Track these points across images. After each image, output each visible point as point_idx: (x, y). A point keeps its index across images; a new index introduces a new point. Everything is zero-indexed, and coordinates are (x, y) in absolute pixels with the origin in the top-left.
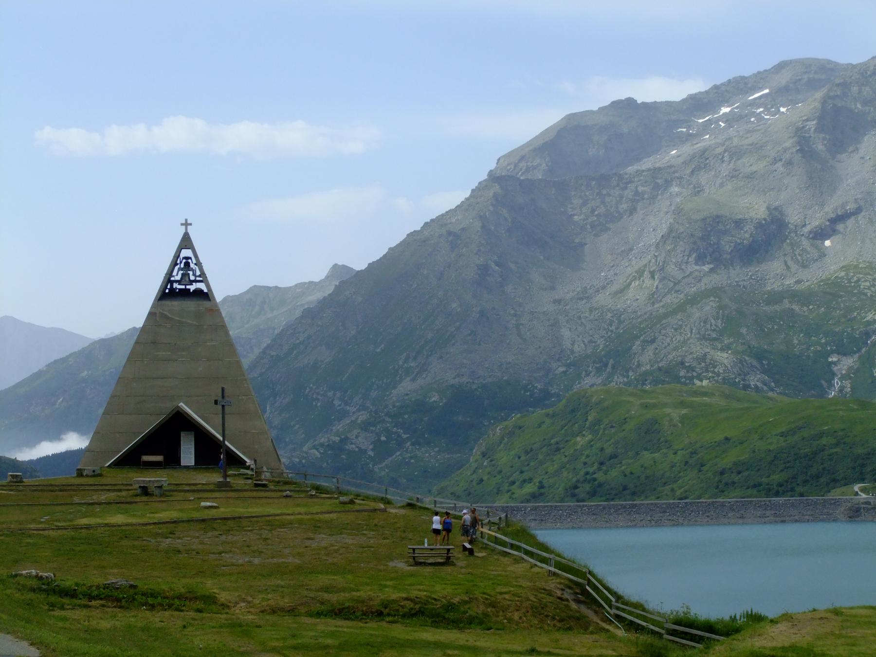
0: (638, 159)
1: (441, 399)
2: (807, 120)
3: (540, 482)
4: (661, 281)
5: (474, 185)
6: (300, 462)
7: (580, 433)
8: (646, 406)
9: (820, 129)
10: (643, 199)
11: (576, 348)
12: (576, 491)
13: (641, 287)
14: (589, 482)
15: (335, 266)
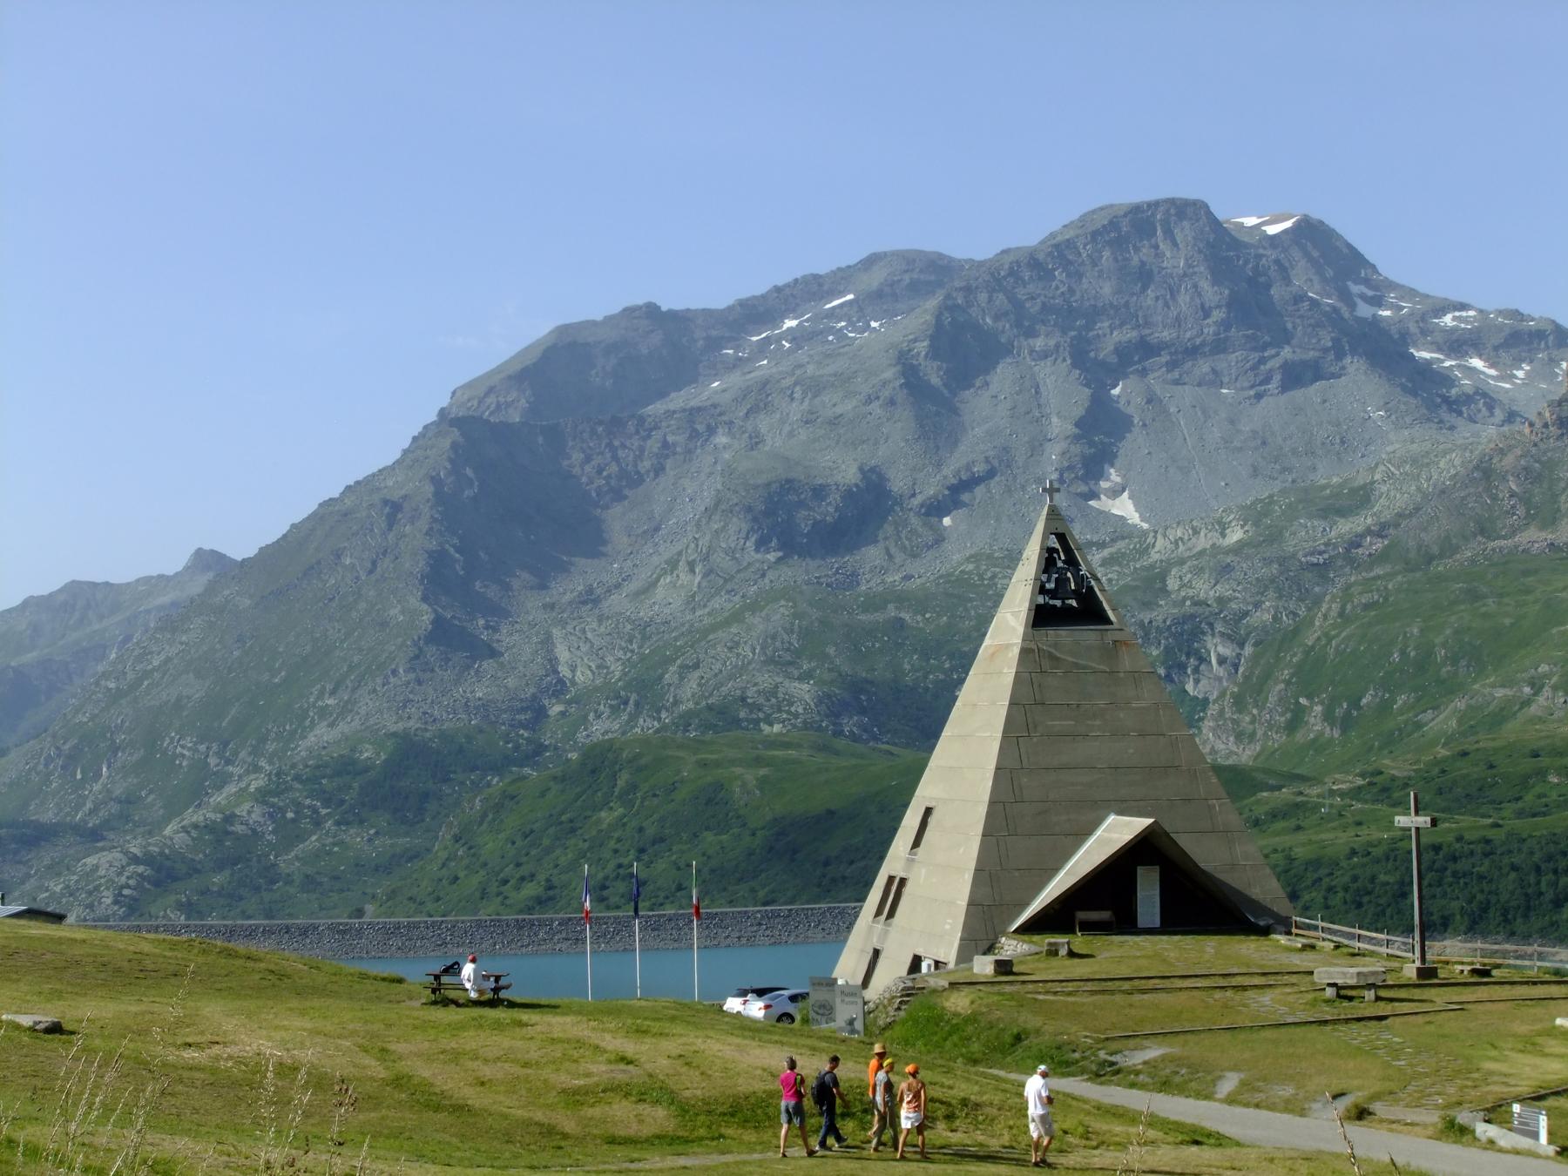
0: (662, 395)
1: (378, 754)
2: (915, 341)
3: (548, 880)
4: (705, 575)
5: (416, 430)
6: (162, 854)
7: (605, 804)
8: (704, 764)
9: (935, 352)
10: (675, 454)
11: (579, 677)
12: (605, 893)
13: (673, 585)
14: (623, 879)
15: (199, 553)
